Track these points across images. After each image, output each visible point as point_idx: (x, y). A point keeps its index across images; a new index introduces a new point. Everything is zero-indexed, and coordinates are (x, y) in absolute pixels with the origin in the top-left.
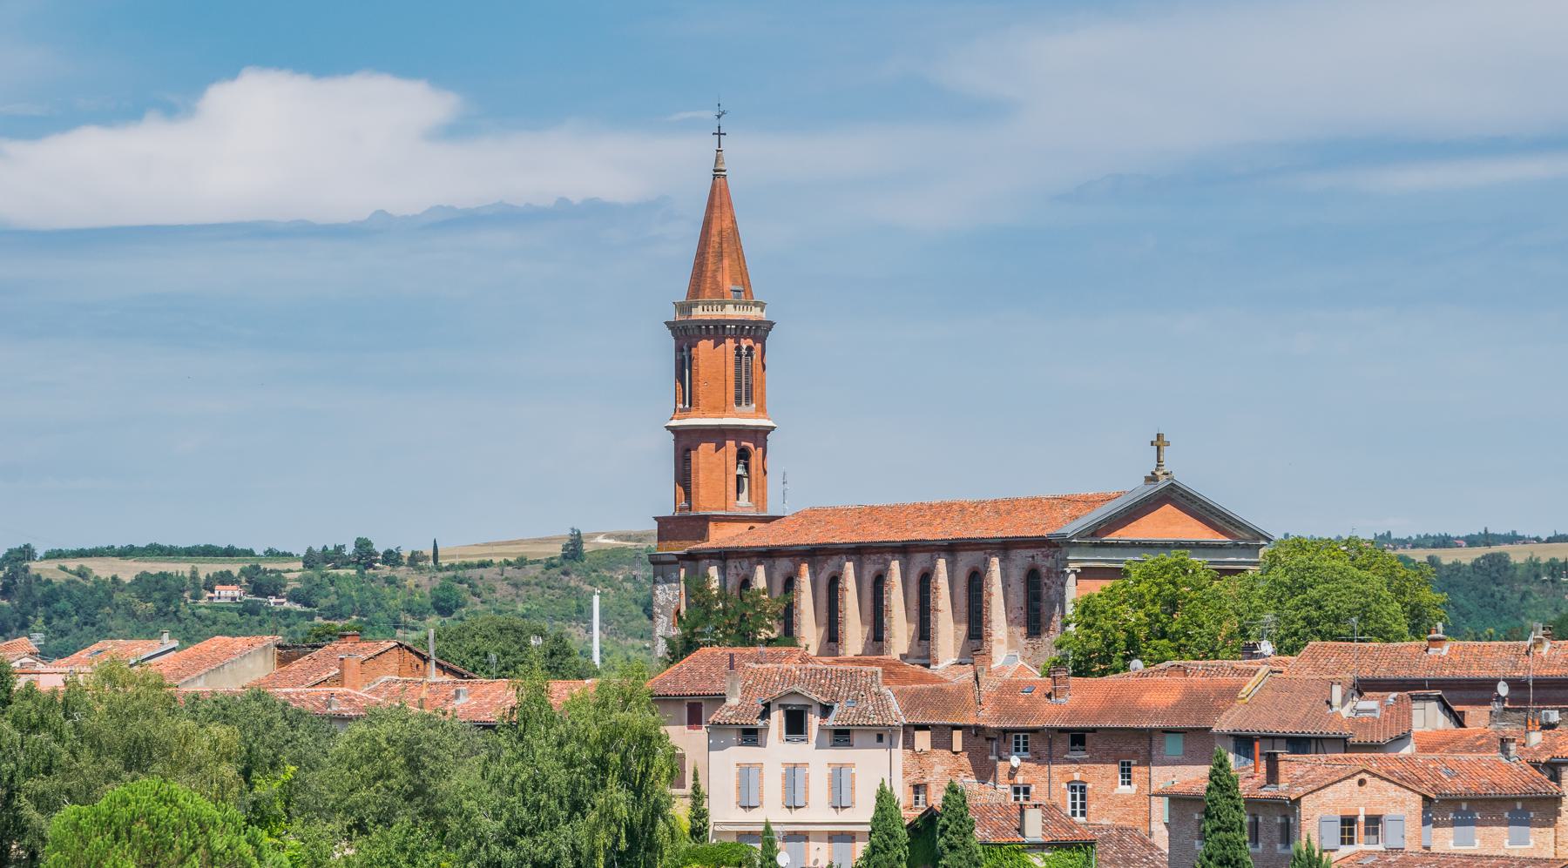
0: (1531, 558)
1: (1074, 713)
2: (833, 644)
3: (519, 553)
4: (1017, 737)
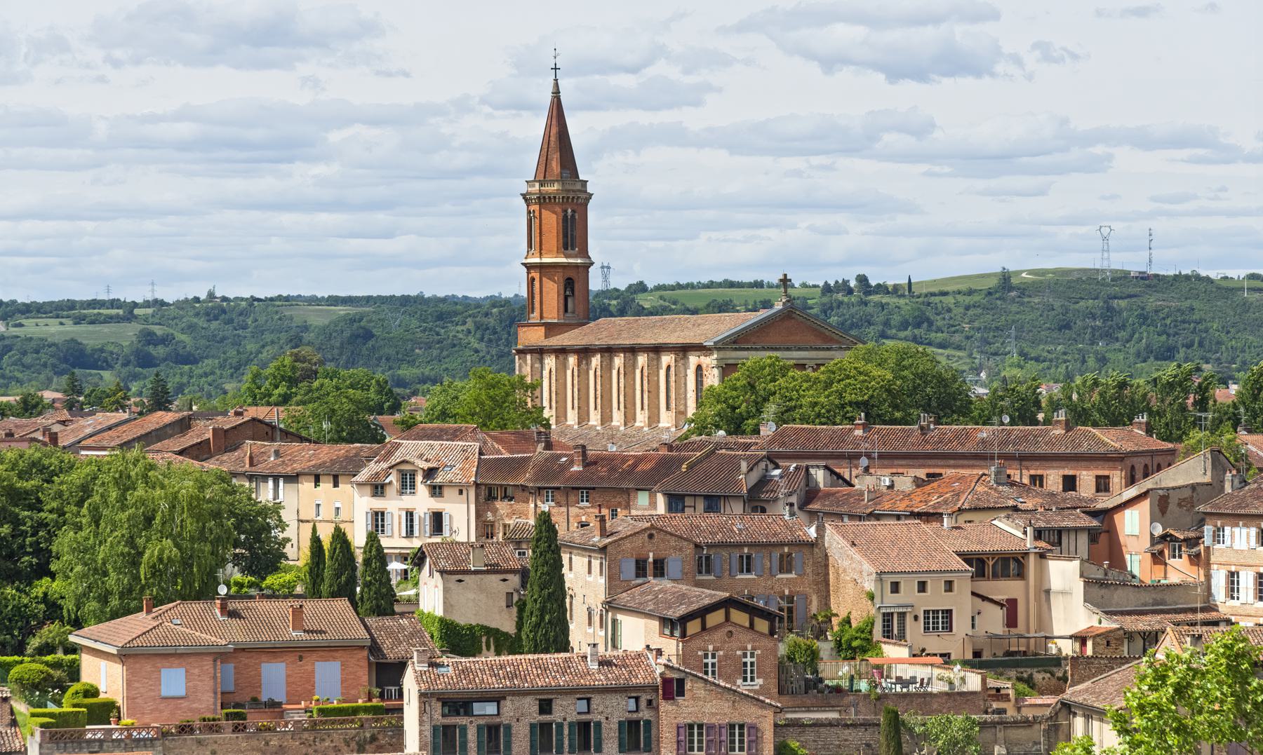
4: (582, 493)
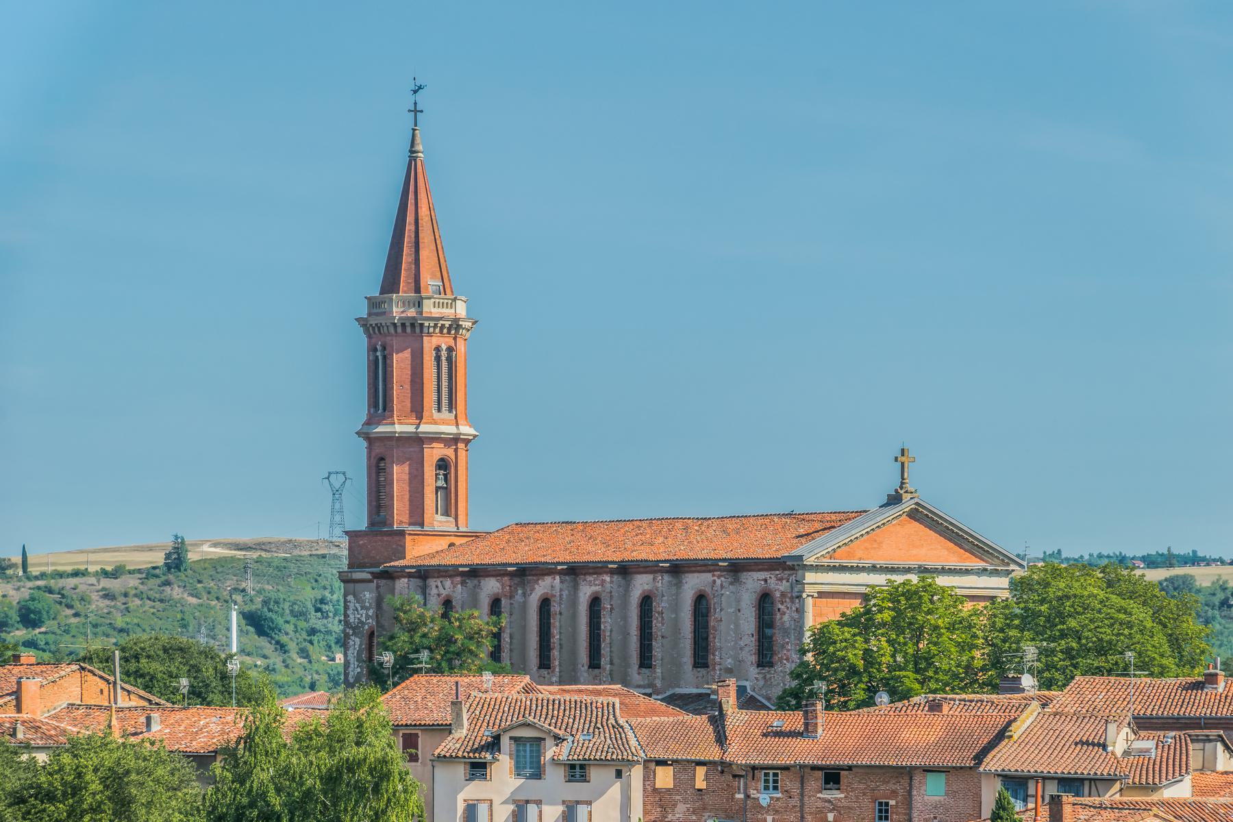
0: (1218, 580)
2: (544, 672)
3: (116, 562)
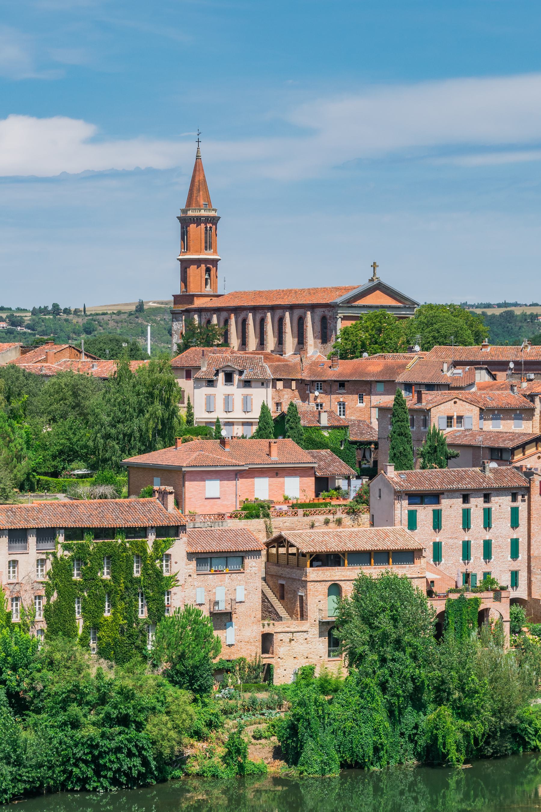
1: (341, 374)
4: (318, 384)
